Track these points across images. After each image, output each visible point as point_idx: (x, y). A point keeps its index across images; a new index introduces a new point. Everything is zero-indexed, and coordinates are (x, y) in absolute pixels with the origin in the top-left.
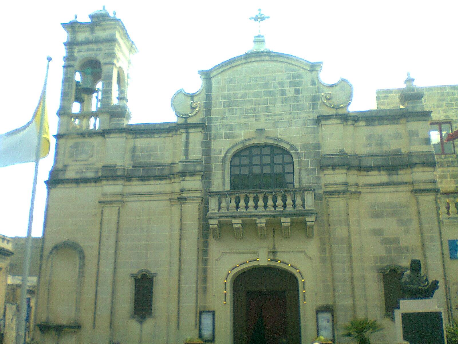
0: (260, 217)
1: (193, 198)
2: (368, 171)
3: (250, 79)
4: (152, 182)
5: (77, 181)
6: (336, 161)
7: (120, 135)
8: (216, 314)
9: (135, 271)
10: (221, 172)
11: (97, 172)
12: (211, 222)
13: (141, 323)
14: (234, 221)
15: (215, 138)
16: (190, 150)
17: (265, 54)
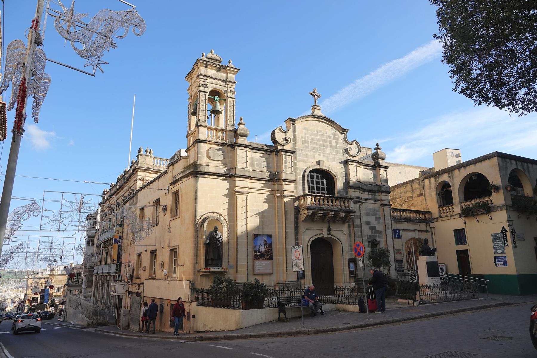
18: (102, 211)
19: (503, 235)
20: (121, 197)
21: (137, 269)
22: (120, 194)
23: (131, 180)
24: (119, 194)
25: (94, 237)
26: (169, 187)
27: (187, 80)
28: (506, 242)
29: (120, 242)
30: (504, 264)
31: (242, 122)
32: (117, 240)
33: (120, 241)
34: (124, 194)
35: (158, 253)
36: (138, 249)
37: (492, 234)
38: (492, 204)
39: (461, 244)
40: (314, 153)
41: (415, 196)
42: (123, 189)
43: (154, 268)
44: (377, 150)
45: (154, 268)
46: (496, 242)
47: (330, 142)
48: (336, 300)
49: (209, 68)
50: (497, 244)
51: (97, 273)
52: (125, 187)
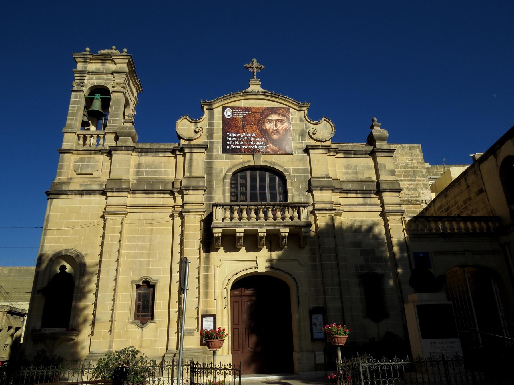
0: (261, 227)
1: (196, 211)
2: (347, 193)
3: (243, 128)
4: (156, 196)
5: (81, 193)
6: (323, 184)
7: (126, 152)
8: (214, 299)
9: (137, 278)
10: (222, 188)
11: (101, 185)
12: (215, 230)
13: (142, 328)
14: (237, 230)
15: (217, 158)
16: (193, 168)
17: (261, 93)
49: (89, 63)
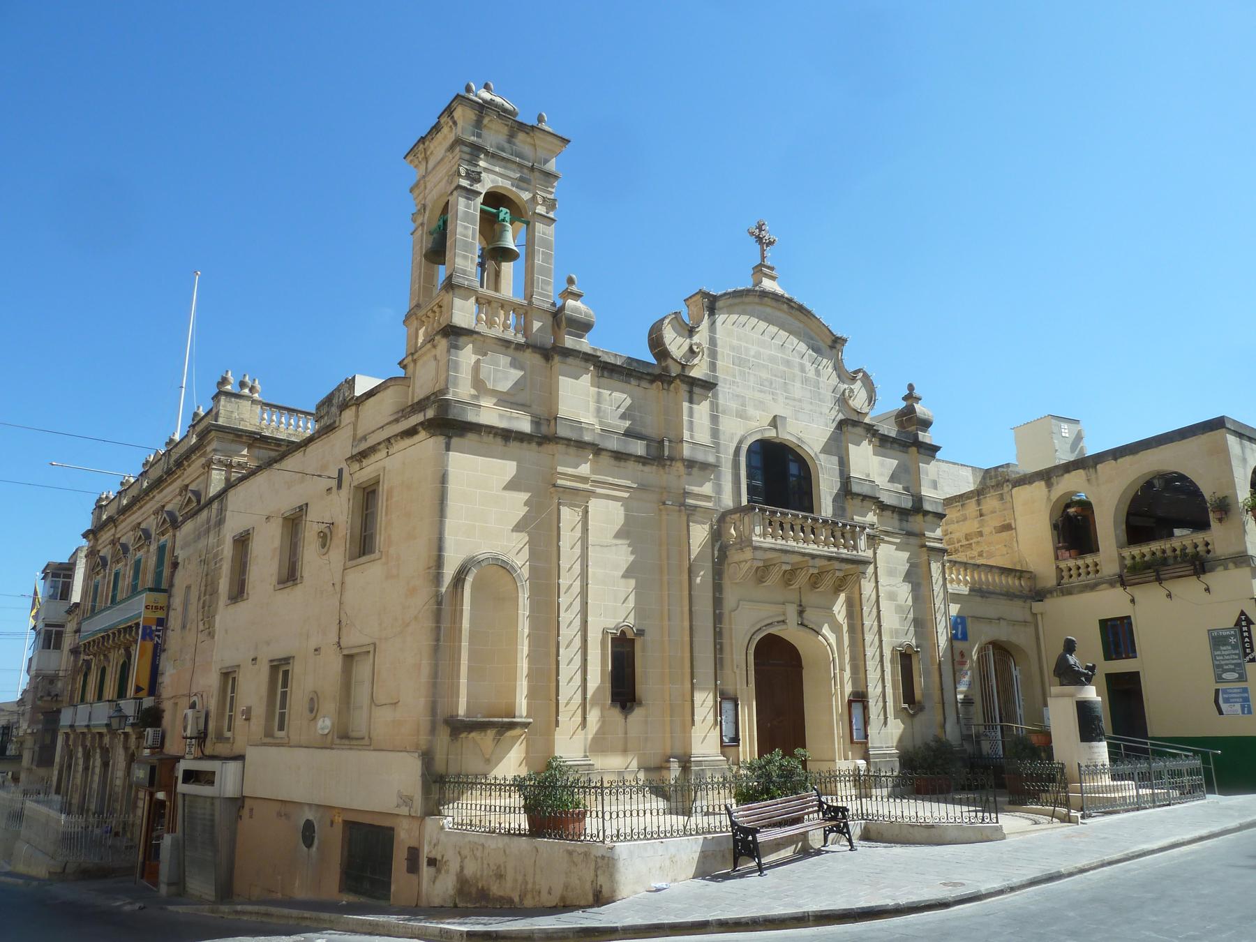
18: (92, 553)
19: (1242, 632)
20: (156, 513)
21: (221, 715)
22: (151, 506)
23: (189, 466)
24: (148, 506)
25: (63, 626)
26: (341, 471)
27: (411, 161)
28: (1248, 651)
29: (158, 636)
30: (1243, 707)
31: (574, 288)
32: (152, 631)
33: (160, 633)
34: (163, 506)
35: (297, 669)
36: (225, 651)
37: (1209, 631)
38: (1208, 552)
39: (1119, 657)
40: (762, 395)
41: (986, 530)
42: (162, 491)
43: (227, 713)
44: (910, 402)
45: (227, 713)
46: (1219, 650)
47: (803, 369)
48: (859, 812)
50: (1223, 655)
51: (72, 726)
52: (170, 484)
